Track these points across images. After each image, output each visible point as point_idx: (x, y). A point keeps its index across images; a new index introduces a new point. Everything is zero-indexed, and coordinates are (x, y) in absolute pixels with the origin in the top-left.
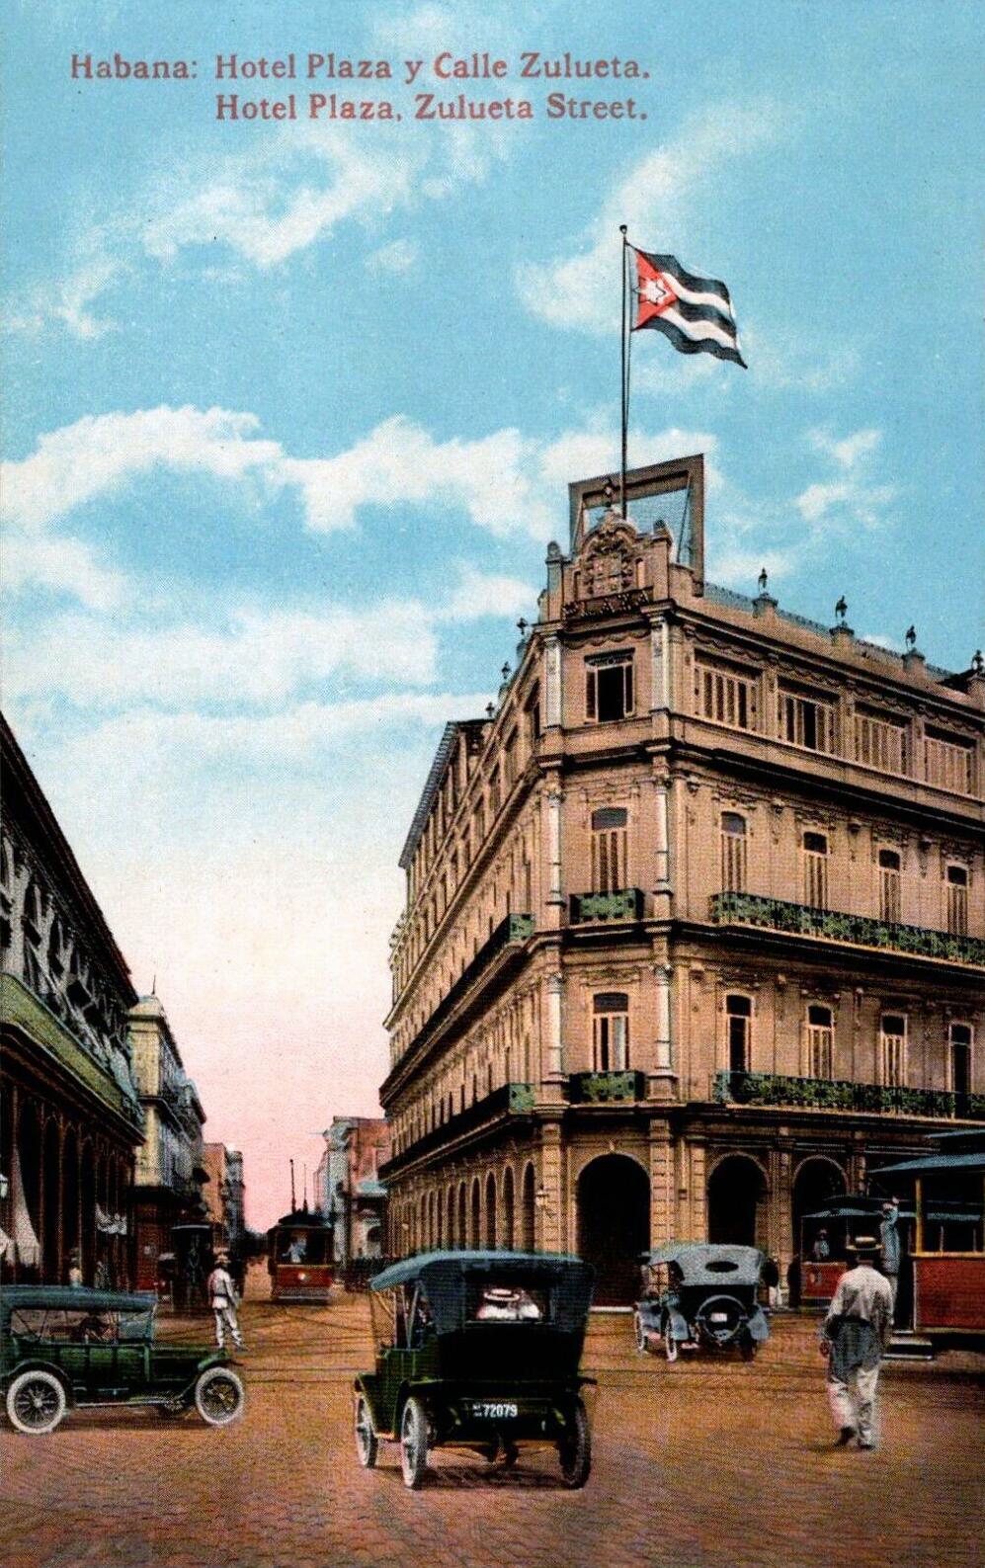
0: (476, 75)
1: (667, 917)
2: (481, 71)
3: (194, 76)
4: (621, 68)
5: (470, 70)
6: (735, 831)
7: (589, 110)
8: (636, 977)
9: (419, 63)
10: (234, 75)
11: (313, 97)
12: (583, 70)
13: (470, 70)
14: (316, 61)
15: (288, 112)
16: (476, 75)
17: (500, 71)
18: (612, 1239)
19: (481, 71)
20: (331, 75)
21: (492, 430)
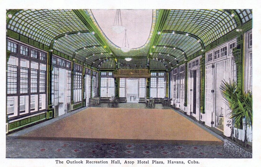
5: (117, 163)
9: (125, 163)
10: (140, 163)
13: (117, 163)
14: (154, 161)
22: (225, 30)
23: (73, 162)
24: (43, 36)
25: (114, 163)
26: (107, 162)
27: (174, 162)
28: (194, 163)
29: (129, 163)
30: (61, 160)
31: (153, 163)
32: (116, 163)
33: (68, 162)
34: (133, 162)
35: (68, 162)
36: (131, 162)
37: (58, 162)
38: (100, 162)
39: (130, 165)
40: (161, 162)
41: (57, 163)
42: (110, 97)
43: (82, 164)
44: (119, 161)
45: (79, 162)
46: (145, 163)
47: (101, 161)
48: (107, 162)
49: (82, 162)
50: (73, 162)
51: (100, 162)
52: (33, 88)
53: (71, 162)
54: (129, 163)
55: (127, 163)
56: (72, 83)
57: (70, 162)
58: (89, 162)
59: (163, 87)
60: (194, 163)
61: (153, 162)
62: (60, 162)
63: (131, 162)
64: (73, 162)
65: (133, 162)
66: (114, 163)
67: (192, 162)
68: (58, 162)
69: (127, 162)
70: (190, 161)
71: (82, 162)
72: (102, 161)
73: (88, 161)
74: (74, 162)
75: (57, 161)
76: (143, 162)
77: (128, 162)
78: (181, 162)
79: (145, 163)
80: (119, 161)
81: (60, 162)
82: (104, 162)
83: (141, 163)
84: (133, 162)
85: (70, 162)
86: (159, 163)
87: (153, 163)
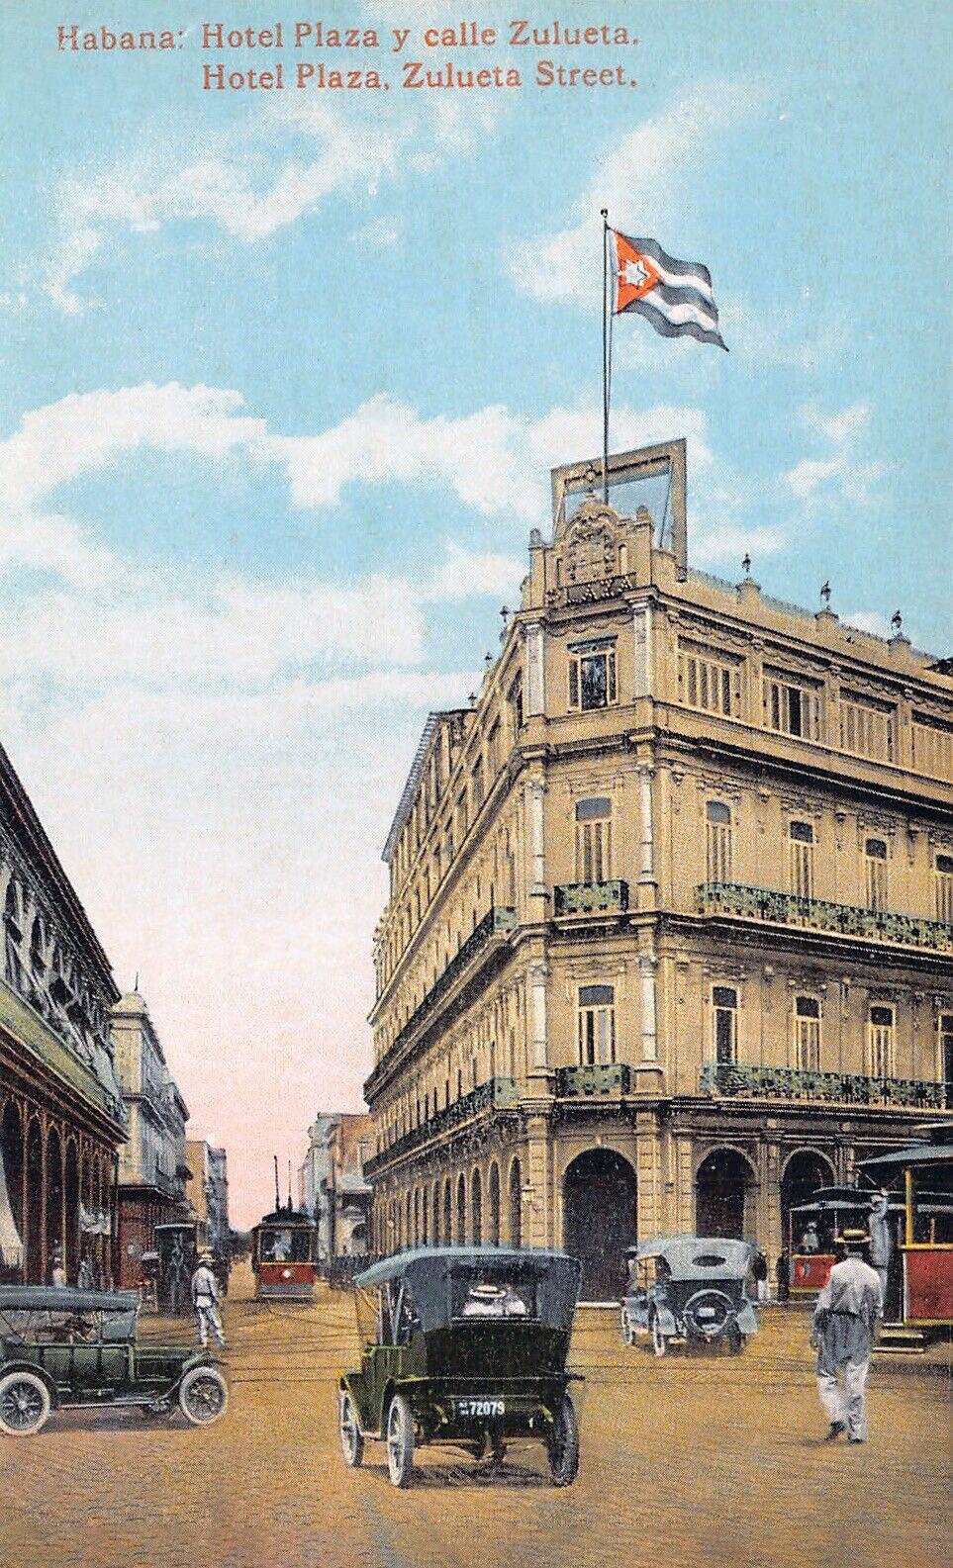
0: (464, 44)
2: (469, 40)
4: (611, 35)
9: (406, 32)
14: (304, 30)
15: (275, 80)
17: (489, 39)
19: (469, 40)
20: (321, 85)
60: (99, 43)
83: (226, 83)
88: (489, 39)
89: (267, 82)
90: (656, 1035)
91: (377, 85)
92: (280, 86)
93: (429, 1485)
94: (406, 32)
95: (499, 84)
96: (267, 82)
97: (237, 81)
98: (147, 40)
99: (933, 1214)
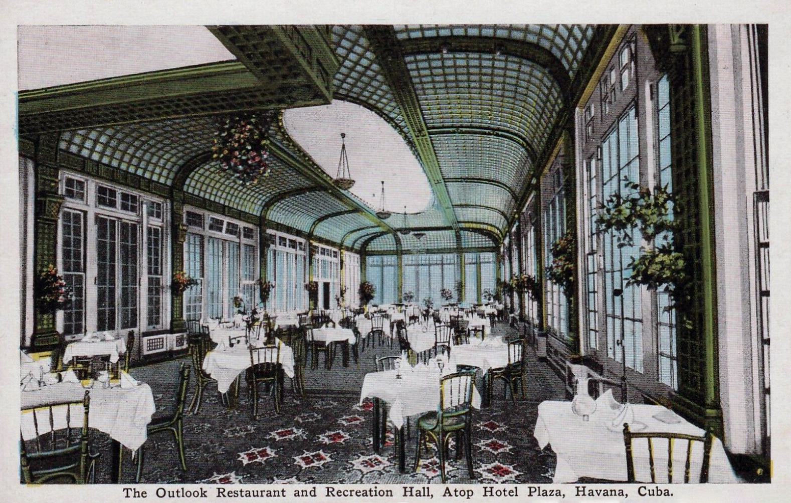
0: (424, 495)
1: (245, 331)
2: (426, 494)
3: (672, 495)
4: (244, 494)
5: (422, 494)
6: (407, 481)
7: (353, 493)
8: (374, 330)
9: (444, 495)
10: (492, 495)
11: (315, 496)
12: (255, 494)
13: (422, 494)
14: (313, 493)
15: (515, 494)
16: (424, 495)
17: (144, 495)
18: (571, 278)
19: (426, 494)
20: (539, 495)
21: (535, 415)
22: (419, 73)
23: (175, 494)
24: (469, 81)
25: (584, 495)
26: (389, 493)
27: (595, 493)
28: (655, 493)
29: (458, 493)
30: (140, 487)
31: (530, 495)
32: (419, 494)
33: (161, 493)
34: (470, 493)
35: (161, 493)
36: (462, 493)
37: (131, 493)
38: (368, 493)
39: (555, 499)
40: (554, 493)
41: (127, 496)
42: (267, 310)
43: (204, 498)
44: (426, 490)
45: (196, 494)
46: (507, 493)
47: (370, 491)
48: (389, 493)
49: (204, 494)
50: (175, 494)
51: (368, 493)
52: (488, 262)
53: (171, 495)
54: (458, 493)
55: (450, 495)
56: (382, 255)
57: (167, 493)
58: (226, 493)
59: (491, 260)
60: (655, 493)
61: (530, 492)
62: (137, 494)
63: (462, 493)
64: (178, 492)
65: (470, 493)
66: (584, 495)
67: (651, 493)
68: (131, 493)
69: (453, 493)
70: (645, 488)
71: (204, 494)
72: (373, 489)
73: (221, 490)
74: (180, 494)
75: (127, 489)
76: (499, 493)
77: (456, 491)
78: (617, 493)
79: (507, 493)
80: (426, 490)
81: (137, 494)
82: (382, 493)
83: (494, 493)
84: (389, 493)
85: (167, 493)
86: (549, 493)
87: (530, 495)
88: (144, 495)
89: (511, 494)
90: (690, 440)
91: (623, 495)
92: (516, 495)
93: (154, 193)
94: (444, 495)
95: (242, 496)
96: (511, 494)
97: (499, 493)
98: (613, 493)
99: (576, 266)
